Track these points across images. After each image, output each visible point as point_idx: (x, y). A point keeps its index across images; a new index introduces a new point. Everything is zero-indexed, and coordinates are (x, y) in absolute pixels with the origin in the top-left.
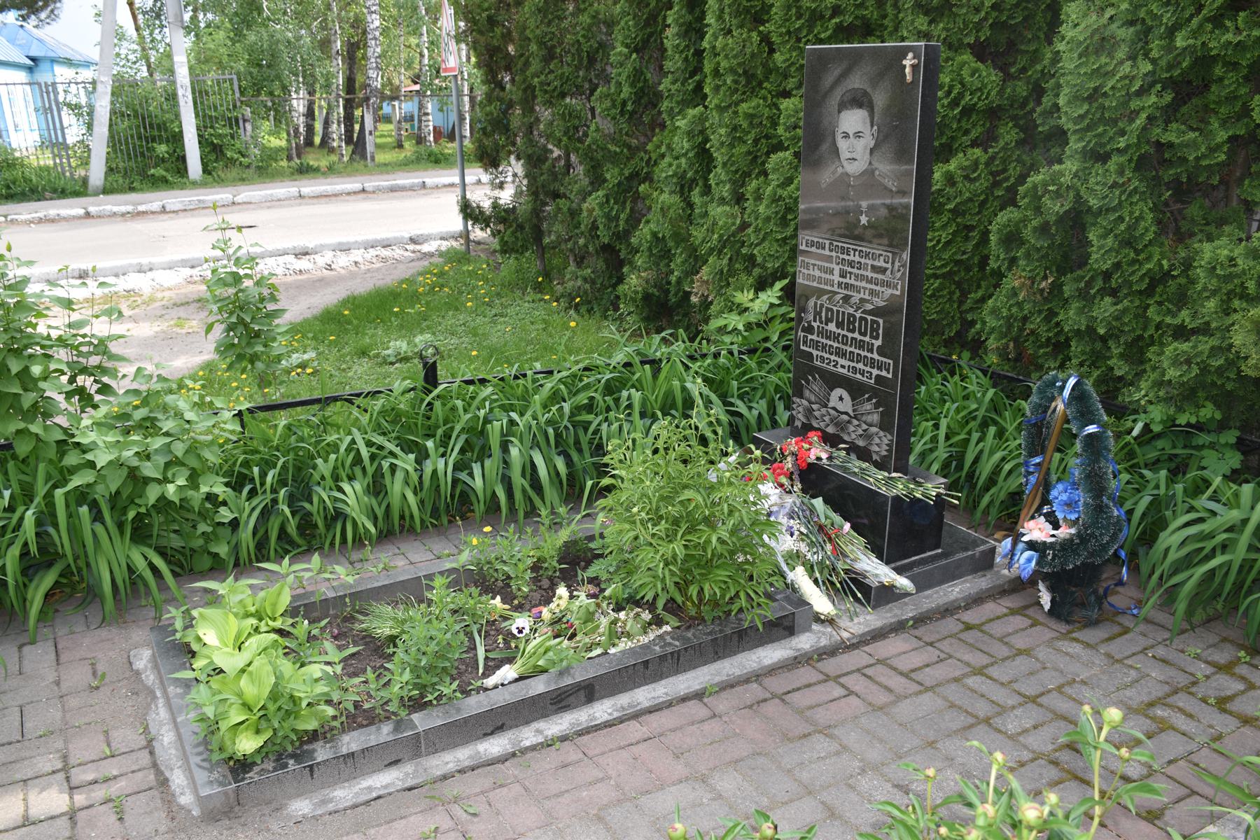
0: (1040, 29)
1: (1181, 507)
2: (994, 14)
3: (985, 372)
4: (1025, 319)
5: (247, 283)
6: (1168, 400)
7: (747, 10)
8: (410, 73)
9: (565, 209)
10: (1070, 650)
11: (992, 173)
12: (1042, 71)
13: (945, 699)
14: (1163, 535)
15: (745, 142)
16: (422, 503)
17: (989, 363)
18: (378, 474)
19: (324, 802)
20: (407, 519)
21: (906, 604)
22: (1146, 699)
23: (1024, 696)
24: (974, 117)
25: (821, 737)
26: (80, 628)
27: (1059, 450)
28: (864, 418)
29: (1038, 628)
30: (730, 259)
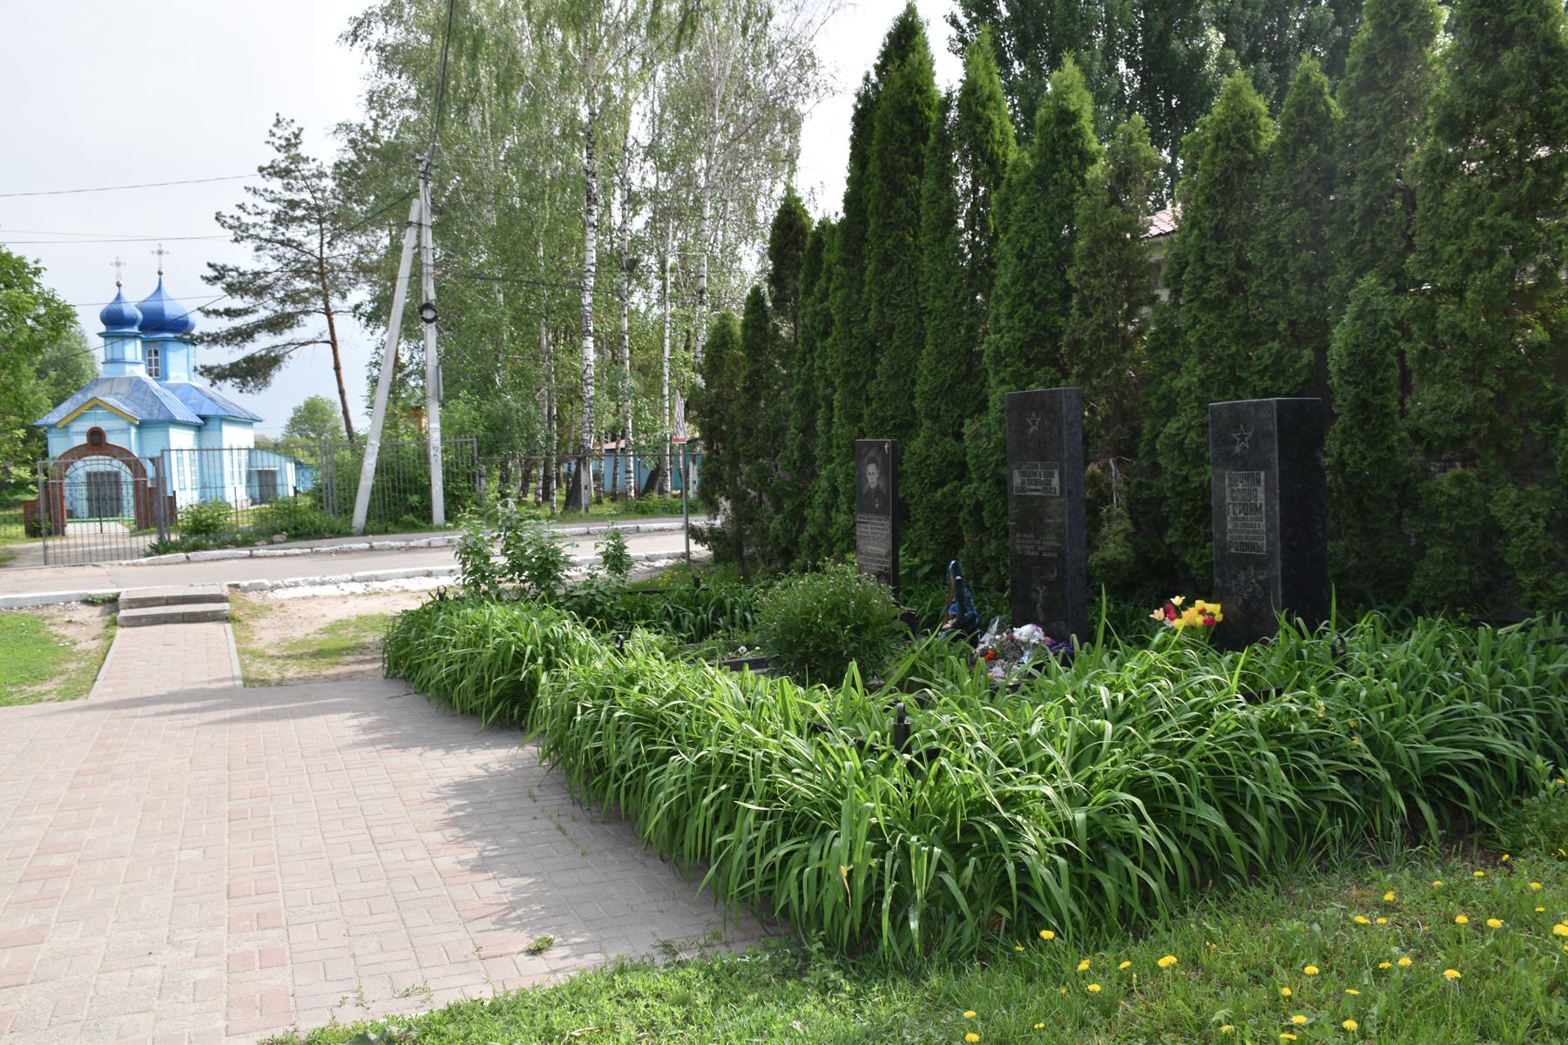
18: (678, 617)
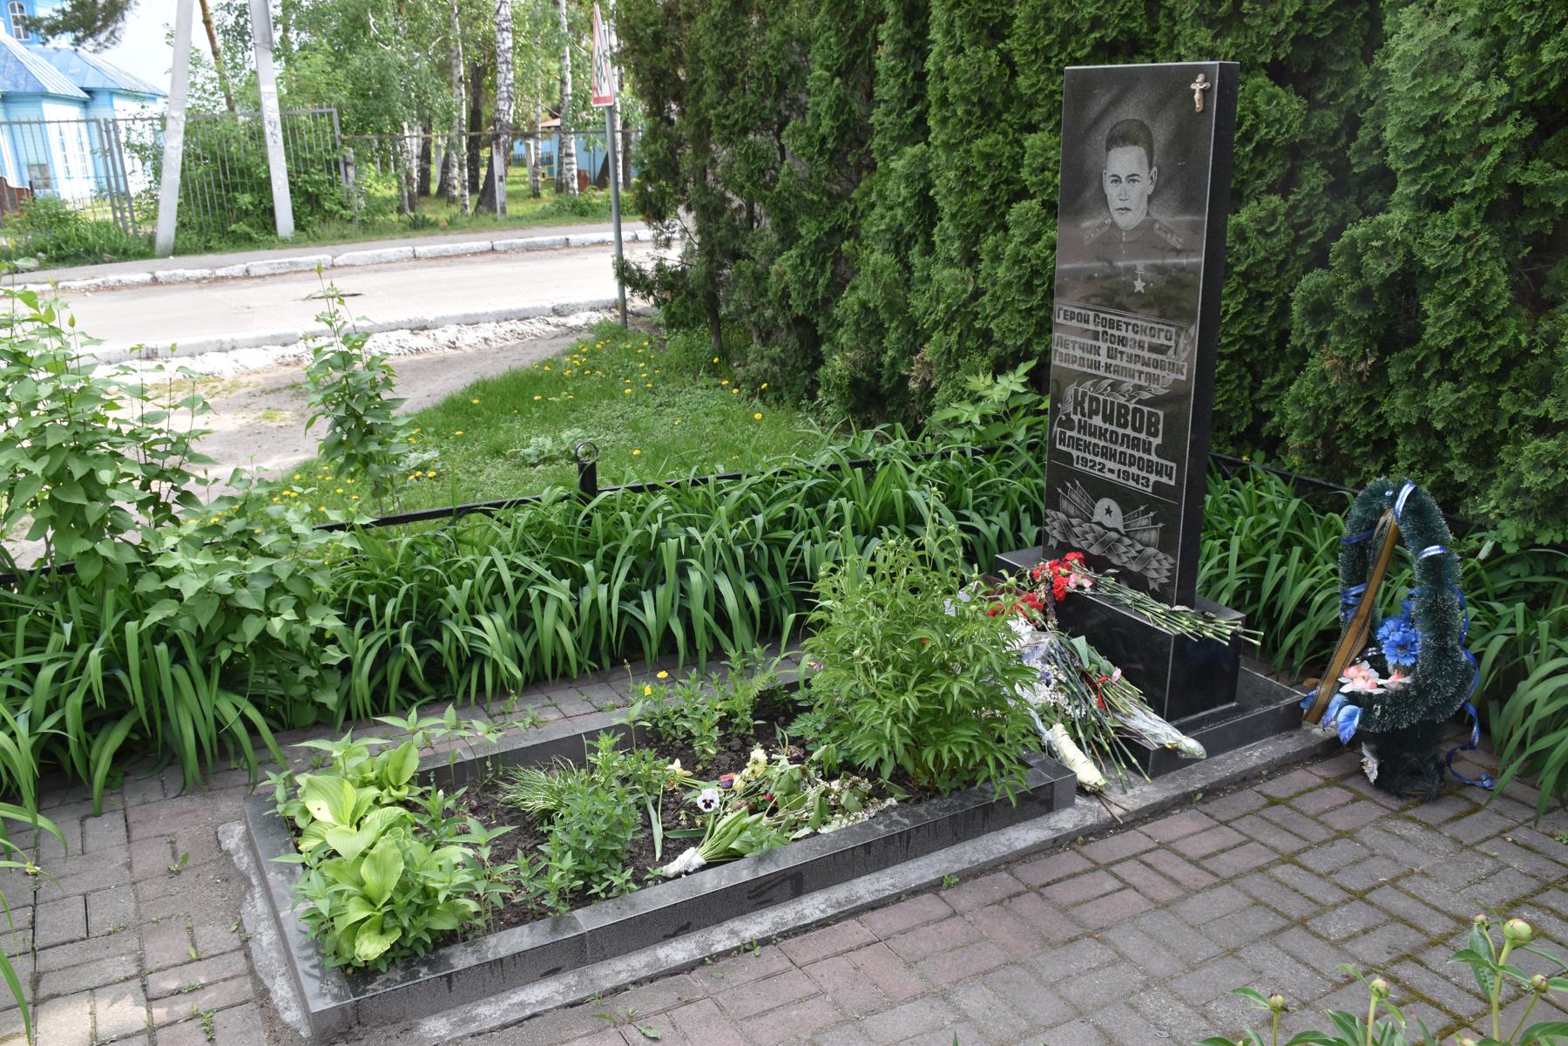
0: (1355, 43)
1: (1544, 650)
2: (1297, 26)
3: (1286, 479)
4: (1337, 410)
5: (358, 365)
6: (1525, 513)
7: (983, 23)
8: (549, 105)
9: (748, 273)
10: (1404, 832)
11: (1293, 226)
12: (1358, 97)
13: (1248, 894)
14: (1523, 686)
15: (979, 188)
16: (578, 641)
17: (1289, 466)
18: (525, 603)
19: (465, 1021)
20: (560, 661)
21: (1193, 772)
22: (1507, 897)
23: (1349, 891)
24: (1271, 156)
25: (1091, 942)
26: (155, 796)
27: (1387, 579)
28: (1138, 536)
29: (1362, 804)
30: (960, 335)
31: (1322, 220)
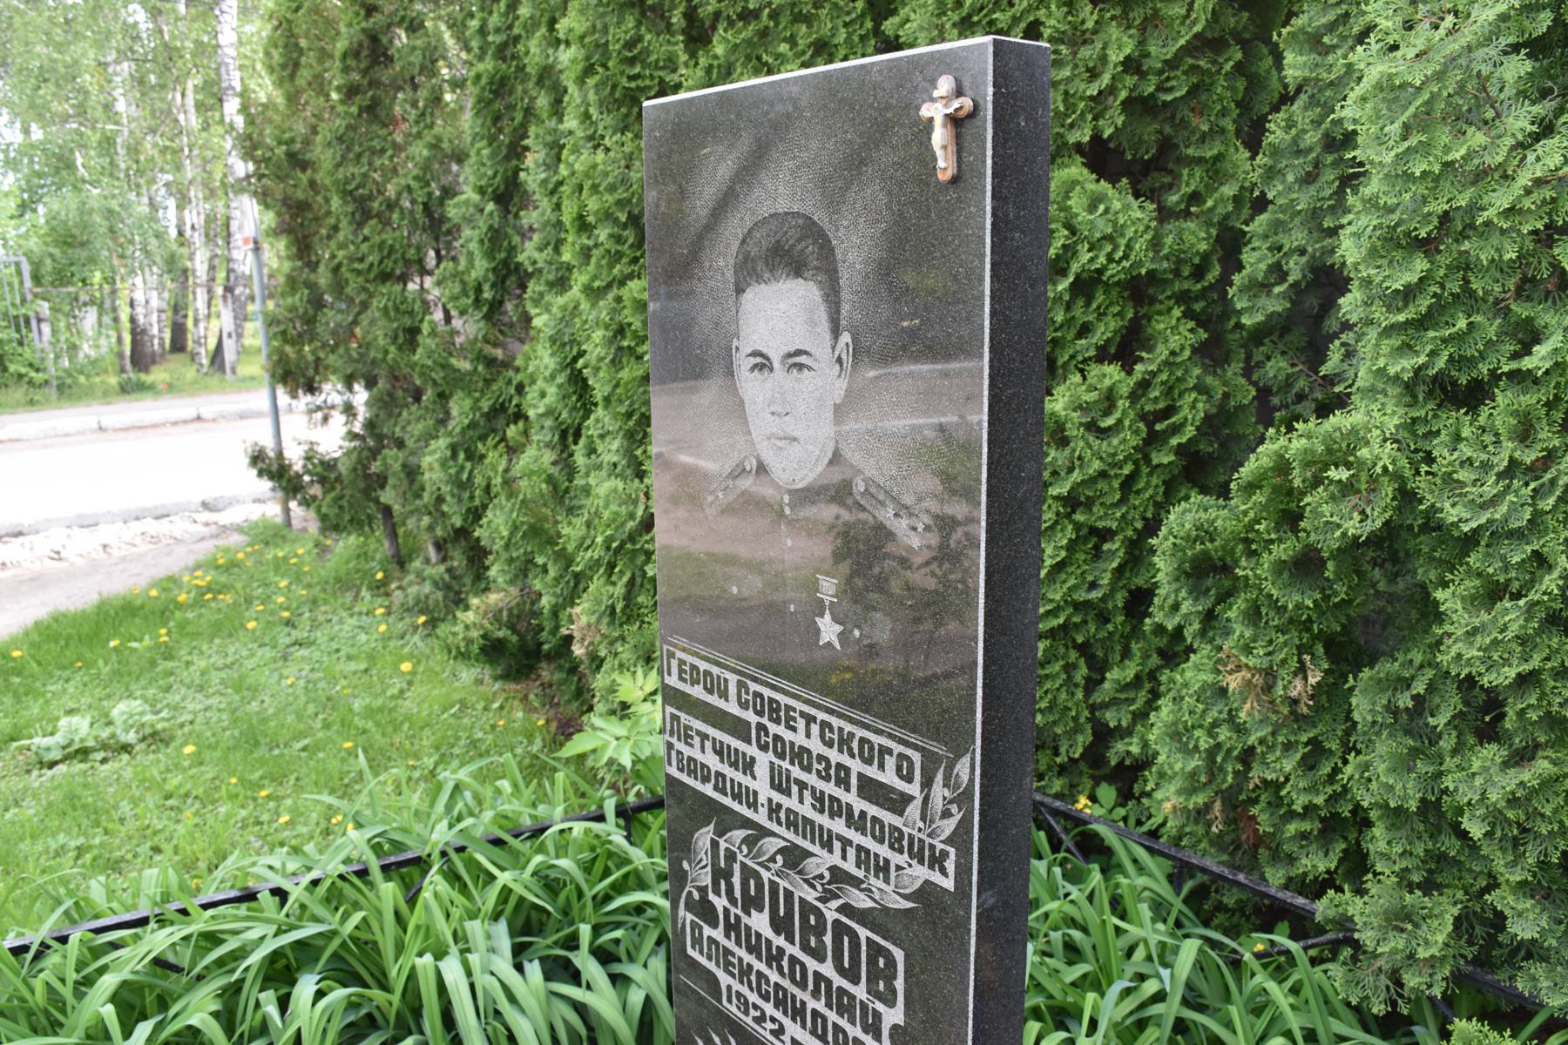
0: (1223, 113)
2: (1130, 80)
4: (1247, 756)
11: (1143, 417)
24: (1100, 298)
31: (1193, 406)
